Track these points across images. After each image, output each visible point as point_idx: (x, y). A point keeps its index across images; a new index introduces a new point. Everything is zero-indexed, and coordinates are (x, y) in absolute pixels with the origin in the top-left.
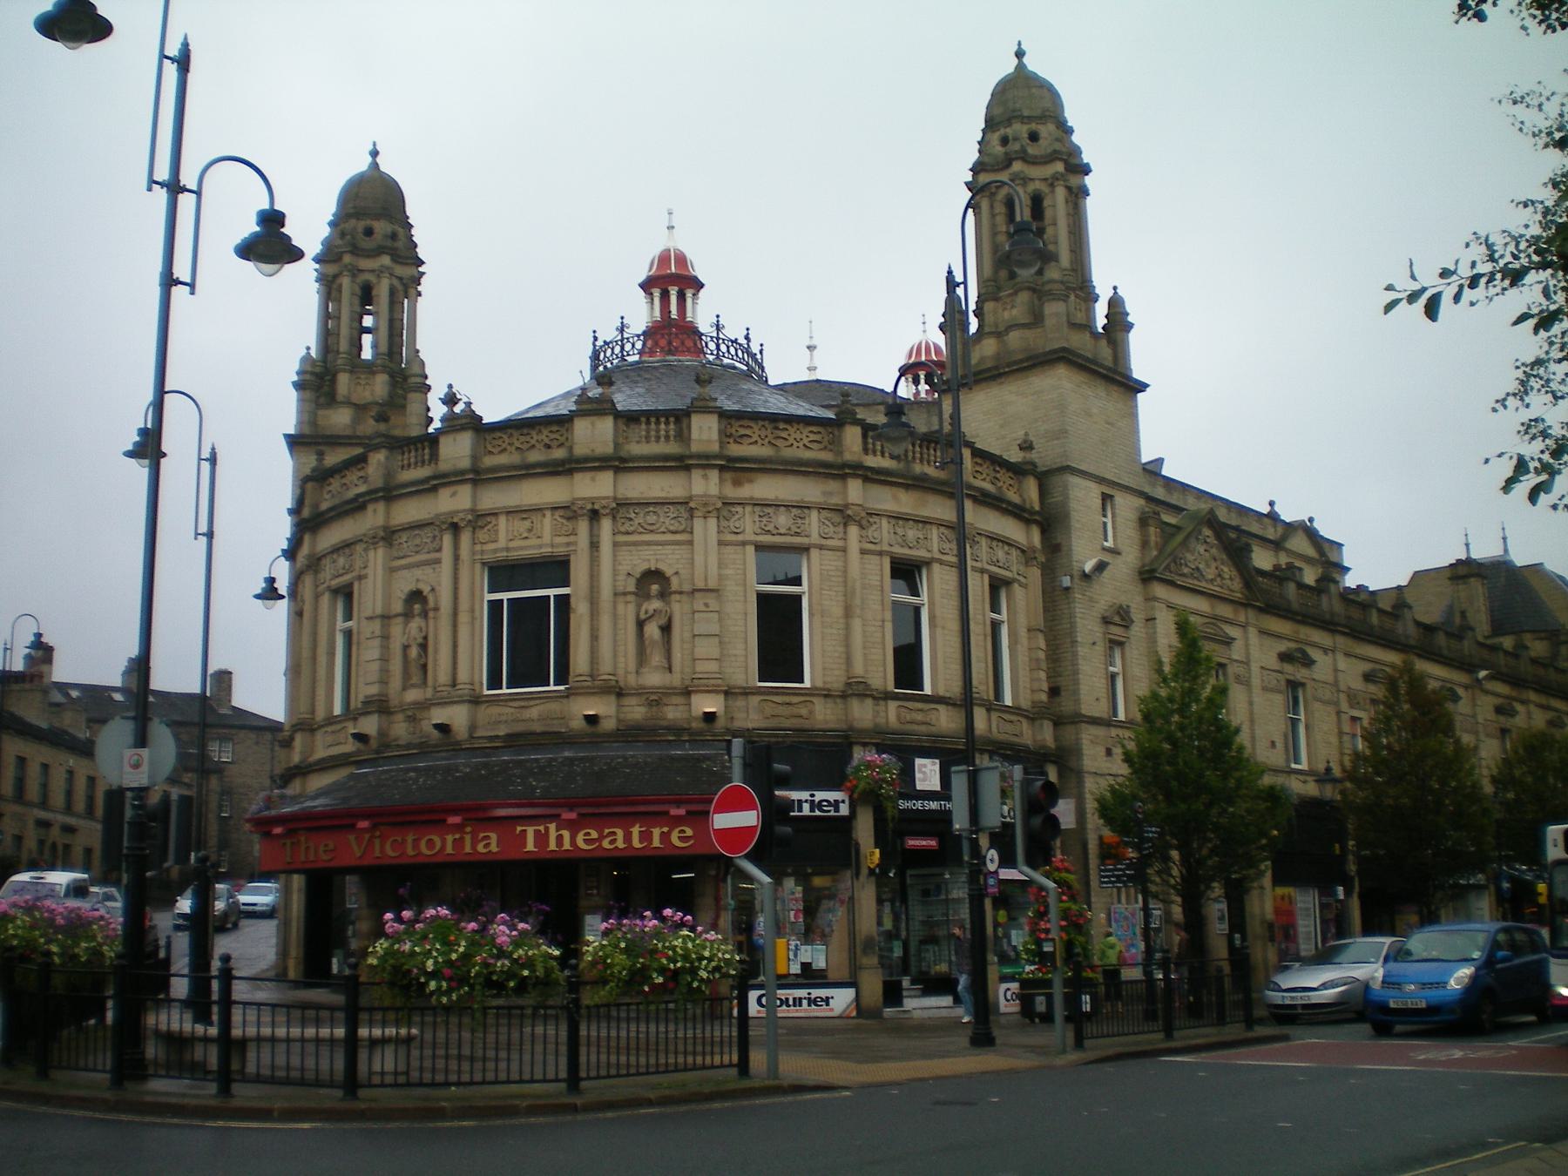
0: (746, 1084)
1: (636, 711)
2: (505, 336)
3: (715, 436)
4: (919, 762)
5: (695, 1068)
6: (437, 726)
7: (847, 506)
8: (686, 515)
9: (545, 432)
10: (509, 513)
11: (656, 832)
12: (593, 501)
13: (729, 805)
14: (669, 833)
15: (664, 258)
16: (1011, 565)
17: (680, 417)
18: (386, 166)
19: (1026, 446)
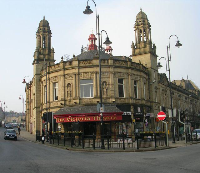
0: (167, 147)
2: (68, 45)
4: (138, 108)
6: (75, 103)
11: (112, 117)
12: (76, 73)
13: (160, 114)
15: (92, 35)
17: (108, 60)
18: (46, 19)
19: (146, 65)
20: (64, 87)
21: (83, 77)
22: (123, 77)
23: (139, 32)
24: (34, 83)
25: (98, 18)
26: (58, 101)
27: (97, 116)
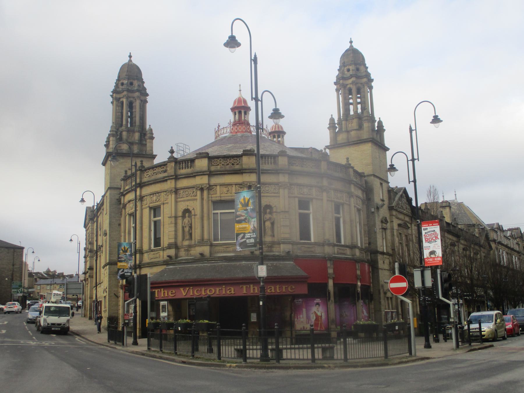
2: (181, 127)
3: (287, 164)
9: (232, 160)
10: (220, 185)
12: (250, 182)
14: (288, 287)
20: (176, 217)
21: (218, 195)
26: (160, 250)
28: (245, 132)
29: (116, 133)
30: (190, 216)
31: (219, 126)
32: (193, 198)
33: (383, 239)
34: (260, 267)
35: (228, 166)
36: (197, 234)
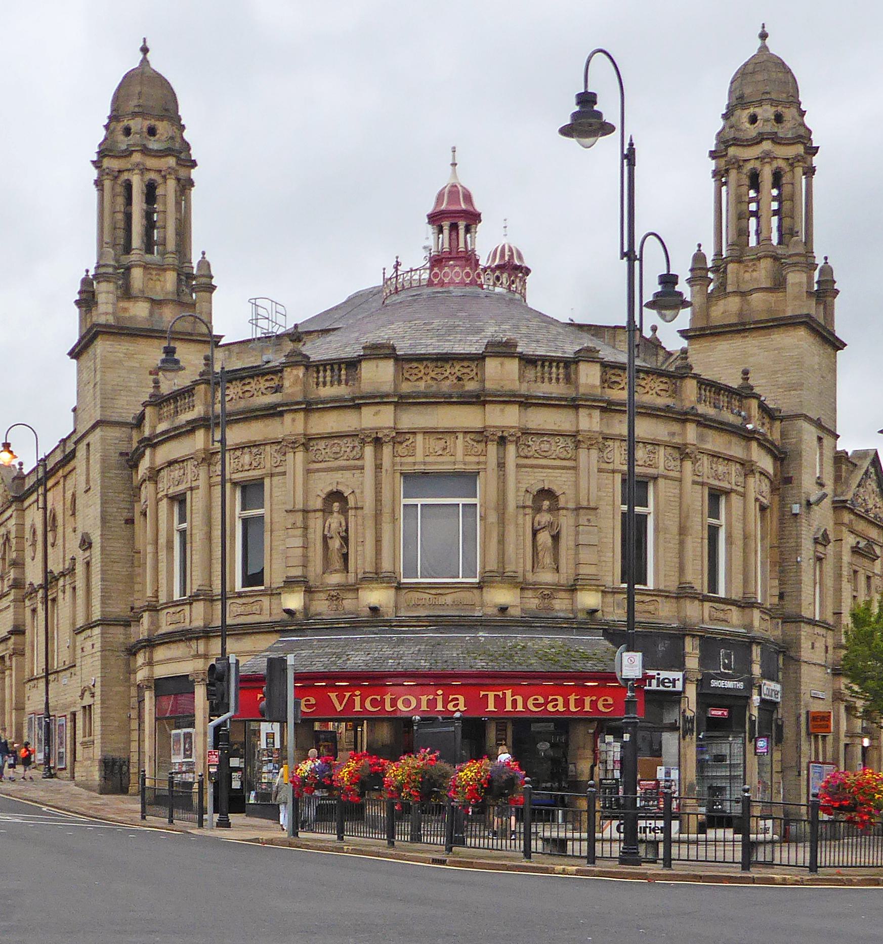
1: (533, 602)
3: (597, 382)
5: (369, 838)
7: (685, 445)
8: (572, 445)
11: (588, 700)
12: (503, 429)
14: (596, 701)
15: (454, 192)
16: (732, 477)
22: (651, 471)
23: (745, 188)
24: (79, 461)
25: (632, 164)
26: (263, 593)
27: (508, 686)
28: (471, 284)
29: (114, 270)
30: (344, 511)
31: (398, 264)
32: (352, 462)
33: (815, 584)
34: (626, 655)
35: (448, 382)
36: (362, 558)
